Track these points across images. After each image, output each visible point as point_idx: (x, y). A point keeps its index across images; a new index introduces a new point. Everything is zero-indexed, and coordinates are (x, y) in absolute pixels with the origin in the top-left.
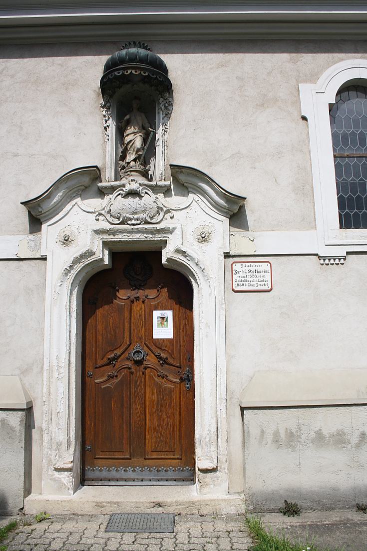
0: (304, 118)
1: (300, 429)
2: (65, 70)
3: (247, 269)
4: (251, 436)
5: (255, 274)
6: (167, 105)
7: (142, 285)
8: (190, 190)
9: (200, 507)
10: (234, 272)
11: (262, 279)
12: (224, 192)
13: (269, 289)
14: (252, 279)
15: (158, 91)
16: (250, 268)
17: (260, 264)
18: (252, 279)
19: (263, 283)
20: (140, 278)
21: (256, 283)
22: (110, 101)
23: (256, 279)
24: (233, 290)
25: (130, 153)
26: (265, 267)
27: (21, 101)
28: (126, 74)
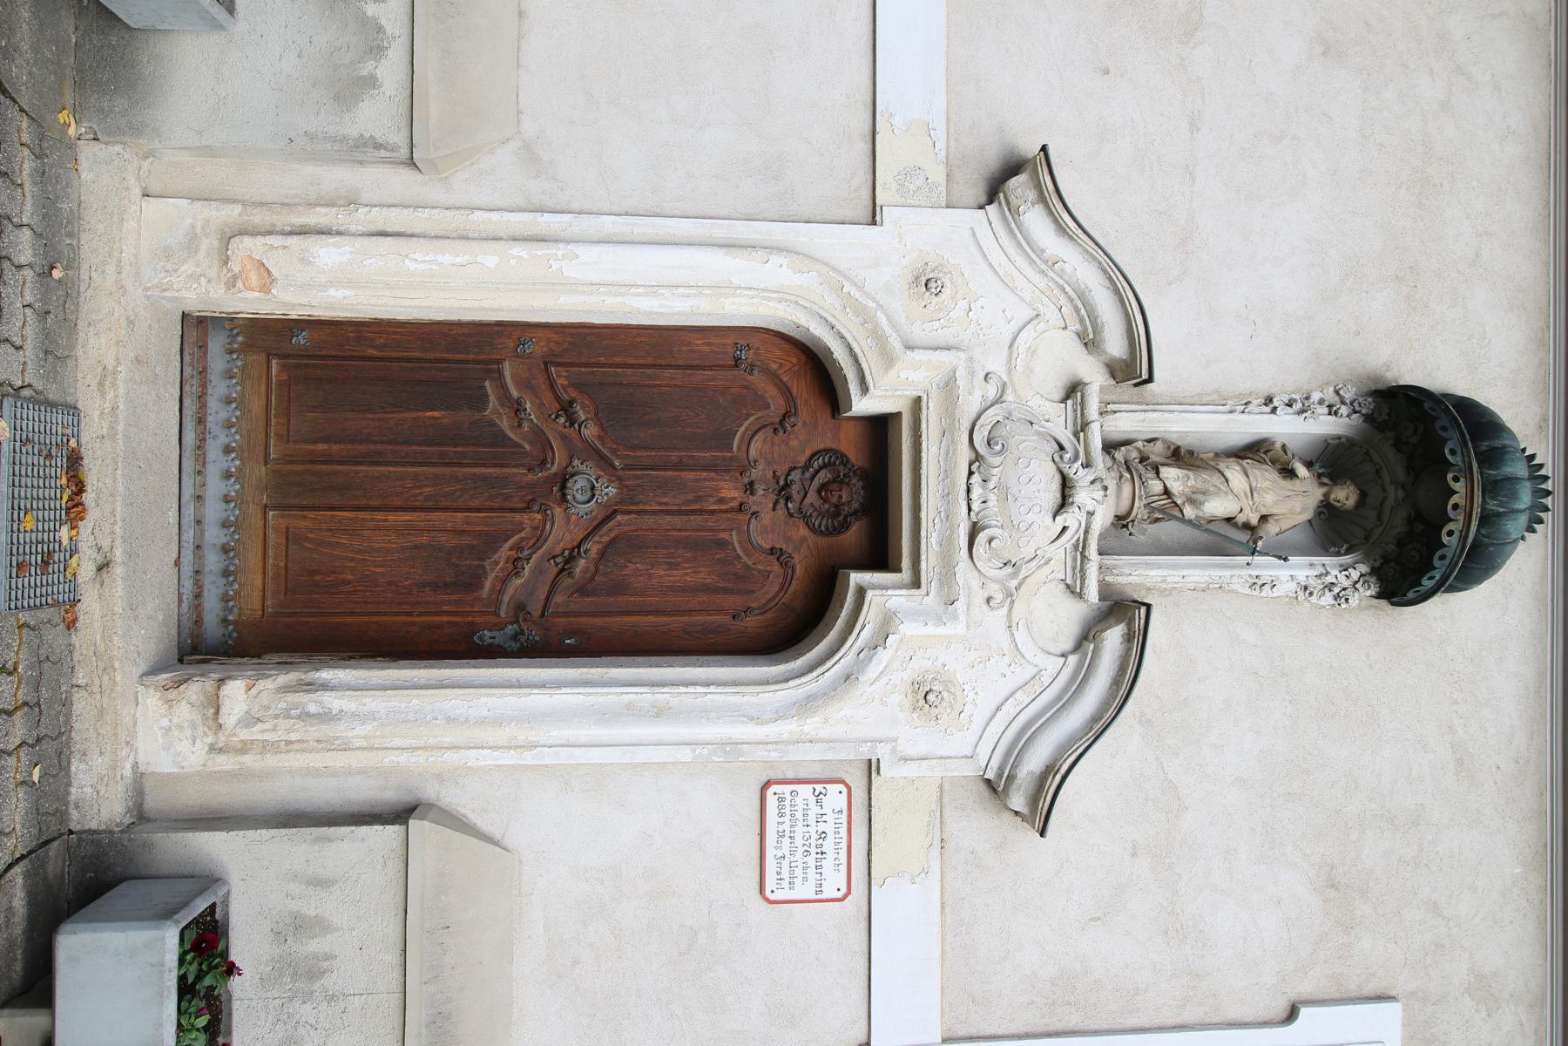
0: (1292, 1015)
1: (331, 998)
2: (1459, 273)
3: (829, 828)
4: (316, 848)
5: (813, 850)
6: (1336, 590)
7: (790, 505)
8: (1073, 659)
9: (96, 689)
10: (819, 788)
11: (799, 872)
12: (1065, 757)
13: (768, 894)
14: (799, 841)
15: (1382, 564)
16: (830, 836)
17: (843, 868)
18: (799, 841)
19: (785, 874)
20: (808, 501)
21: (787, 855)
22: (1355, 416)
23: (799, 854)
24: (768, 784)
25: (1189, 478)
26: (834, 883)
27: (1364, 136)
28: (1450, 476)
